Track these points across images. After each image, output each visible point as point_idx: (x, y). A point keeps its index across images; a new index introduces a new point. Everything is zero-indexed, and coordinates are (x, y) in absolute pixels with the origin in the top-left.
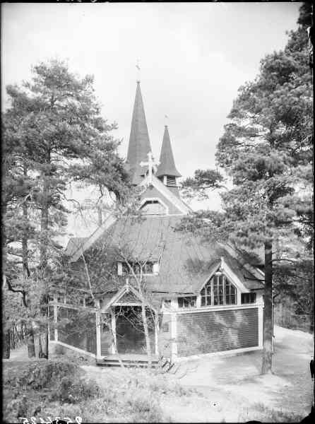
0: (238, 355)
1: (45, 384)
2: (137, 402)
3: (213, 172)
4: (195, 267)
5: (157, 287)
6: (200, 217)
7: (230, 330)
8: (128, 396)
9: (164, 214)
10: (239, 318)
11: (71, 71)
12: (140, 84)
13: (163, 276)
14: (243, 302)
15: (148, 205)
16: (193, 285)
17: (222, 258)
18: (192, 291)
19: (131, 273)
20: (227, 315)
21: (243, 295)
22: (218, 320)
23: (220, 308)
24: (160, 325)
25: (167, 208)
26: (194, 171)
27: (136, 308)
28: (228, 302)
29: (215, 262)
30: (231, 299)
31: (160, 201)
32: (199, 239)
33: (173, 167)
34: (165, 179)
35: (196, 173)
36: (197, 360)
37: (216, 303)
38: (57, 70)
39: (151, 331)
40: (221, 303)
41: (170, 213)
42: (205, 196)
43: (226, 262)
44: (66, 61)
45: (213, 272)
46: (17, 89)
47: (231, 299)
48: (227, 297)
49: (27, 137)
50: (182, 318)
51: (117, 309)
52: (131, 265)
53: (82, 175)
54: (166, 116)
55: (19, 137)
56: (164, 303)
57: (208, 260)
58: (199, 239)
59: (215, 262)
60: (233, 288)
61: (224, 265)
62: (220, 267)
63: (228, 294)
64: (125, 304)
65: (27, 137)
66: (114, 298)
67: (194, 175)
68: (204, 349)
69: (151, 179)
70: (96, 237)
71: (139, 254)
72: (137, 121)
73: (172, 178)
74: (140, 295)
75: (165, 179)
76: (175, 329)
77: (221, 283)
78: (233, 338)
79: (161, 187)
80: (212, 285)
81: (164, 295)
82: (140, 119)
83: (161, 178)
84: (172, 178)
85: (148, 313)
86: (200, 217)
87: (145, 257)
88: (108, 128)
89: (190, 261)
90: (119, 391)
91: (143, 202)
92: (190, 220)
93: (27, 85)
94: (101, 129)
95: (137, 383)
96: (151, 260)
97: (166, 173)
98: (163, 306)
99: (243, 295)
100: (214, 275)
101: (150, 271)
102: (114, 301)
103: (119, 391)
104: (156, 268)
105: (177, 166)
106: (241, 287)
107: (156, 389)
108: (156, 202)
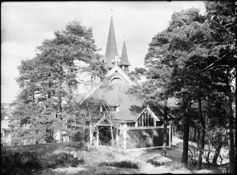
0: (154, 149)
1: (80, 147)
2: (108, 153)
3: (142, 69)
4: (135, 109)
5: (117, 118)
6: (136, 88)
7: (150, 138)
8: (106, 152)
9: (122, 84)
10: (155, 133)
11: (82, 25)
12: (113, 18)
13: (120, 113)
14: (157, 125)
15: (115, 79)
16: (134, 118)
17: (148, 105)
18: (133, 120)
19: (106, 111)
20: (150, 132)
21: (157, 122)
22: (144, 134)
23: (146, 128)
24: (119, 135)
25: (124, 81)
26: (135, 68)
27: (108, 126)
28: (150, 126)
29: (144, 107)
30: (152, 124)
31: (120, 78)
32: (135, 98)
33: (127, 61)
34: (123, 67)
35: (152, 38)
36: (135, 151)
37: (144, 126)
38: (77, 26)
39: (115, 137)
40: (147, 126)
41: (125, 84)
42: (139, 78)
43: (149, 107)
44: (80, 22)
45: (143, 111)
46: (59, 33)
47: (152, 124)
48: (144, 123)
49: (65, 56)
50: (129, 133)
51: (100, 127)
52: (106, 108)
53: (84, 70)
54: (124, 37)
55: (62, 56)
56: (121, 125)
57: (141, 106)
58: (135, 98)
59: (144, 107)
60: (152, 119)
61: (148, 109)
62: (146, 109)
63: (150, 122)
64: (103, 125)
65: (65, 56)
66: (98, 123)
67: (135, 70)
68: (139, 147)
69: (116, 68)
70: (91, 93)
71: (109, 103)
72: (110, 36)
73: (126, 66)
74: (110, 121)
75: (123, 67)
76: (125, 135)
77: (147, 116)
78: (151, 141)
79: (121, 71)
80: (143, 117)
81: (120, 121)
82: (112, 35)
83: (121, 66)
84: (126, 66)
85: (113, 128)
86: (136, 88)
87: (113, 104)
88: (98, 50)
89: (132, 106)
90: (102, 151)
91: (112, 78)
92: (132, 90)
93: (64, 32)
94: (95, 50)
95: (108, 149)
96: (116, 105)
97: (124, 64)
98: (120, 126)
99: (157, 122)
100: (143, 113)
101: (115, 110)
102: (99, 124)
103: (102, 151)
104: (117, 109)
105: (129, 61)
106: (156, 119)
107: (115, 152)
108: (119, 78)
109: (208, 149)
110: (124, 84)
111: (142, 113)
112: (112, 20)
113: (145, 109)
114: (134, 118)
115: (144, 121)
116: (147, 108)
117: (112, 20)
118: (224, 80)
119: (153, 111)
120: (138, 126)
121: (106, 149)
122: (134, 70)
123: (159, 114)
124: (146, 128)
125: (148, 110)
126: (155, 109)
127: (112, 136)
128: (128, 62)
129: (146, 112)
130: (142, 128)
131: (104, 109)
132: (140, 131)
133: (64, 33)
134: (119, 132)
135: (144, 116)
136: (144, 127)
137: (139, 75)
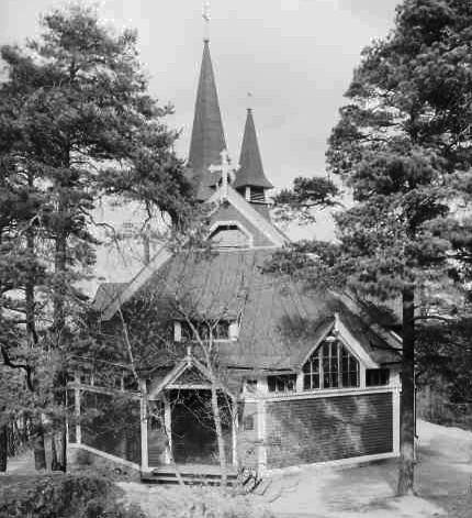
0: (361, 465)
3: (322, 181)
4: (294, 328)
5: (235, 360)
6: (302, 250)
7: (349, 427)
9: (246, 247)
10: (363, 408)
13: (245, 343)
14: (368, 383)
21: (369, 372)
22: (331, 411)
23: (333, 392)
24: (239, 420)
25: (251, 237)
26: (293, 179)
27: (202, 392)
28: (345, 384)
29: (325, 321)
30: (351, 380)
31: (240, 226)
32: (300, 285)
33: (260, 172)
34: (248, 191)
36: (297, 474)
37: (326, 385)
38: (79, 22)
39: (226, 428)
43: (342, 321)
44: (94, 9)
46: (17, 51)
50: (274, 408)
51: (173, 394)
52: (197, 326)
54: (249, 94)
57: (314, 317)
58: (300, 285)
61: (339, 326)
62: (333, 328)
63: (346, 370)
65: (32, 126)
68: (308, 457)
69: (225, 192)
71: (207, 308)
72: (204, 101)
74: (209, 373)
75: (248, 191)
76: (263, 426)
77: (334, 353)
78: (354, 438)
81: (247, 372)
82: (208, 71)
83: (241, 190)
85: (222, 400)
87: (216, 313)
88: (159, 113)
89: (286, 320)
93: (34, 46)
94: (148, 114)
95: (205, 509)
97: (250, 183)
98: (245, 389)
99: (369, 372)
101: (225, 334)
104: (234, 330)
106: (366, 360)
108: (234, 228)
109: (36, 240)
110: (252, 247)
111: (320, 341)
112: (206, 47)
113: (329, 328)
114: (291, 357)
115: (326, 369)
116: (336, 326)
117: (206, 47)
118: (415, 261)
119: (355, 334)
120: (307, 385)
121: (194, 508)
122: (290, 187)
123: (376, 344)
124: (333, 392)
125: (338, 333)
126: (370, 324)
127: (219, 430)
128: (264, 177)
129: (331, 338)
130: (321, 392)
131: (187, 333)
132: (312, 403)
133: (32, 47)
134: (240, 412)
135: (326, 353)
136: (326, 391)
137: (308, 207)
